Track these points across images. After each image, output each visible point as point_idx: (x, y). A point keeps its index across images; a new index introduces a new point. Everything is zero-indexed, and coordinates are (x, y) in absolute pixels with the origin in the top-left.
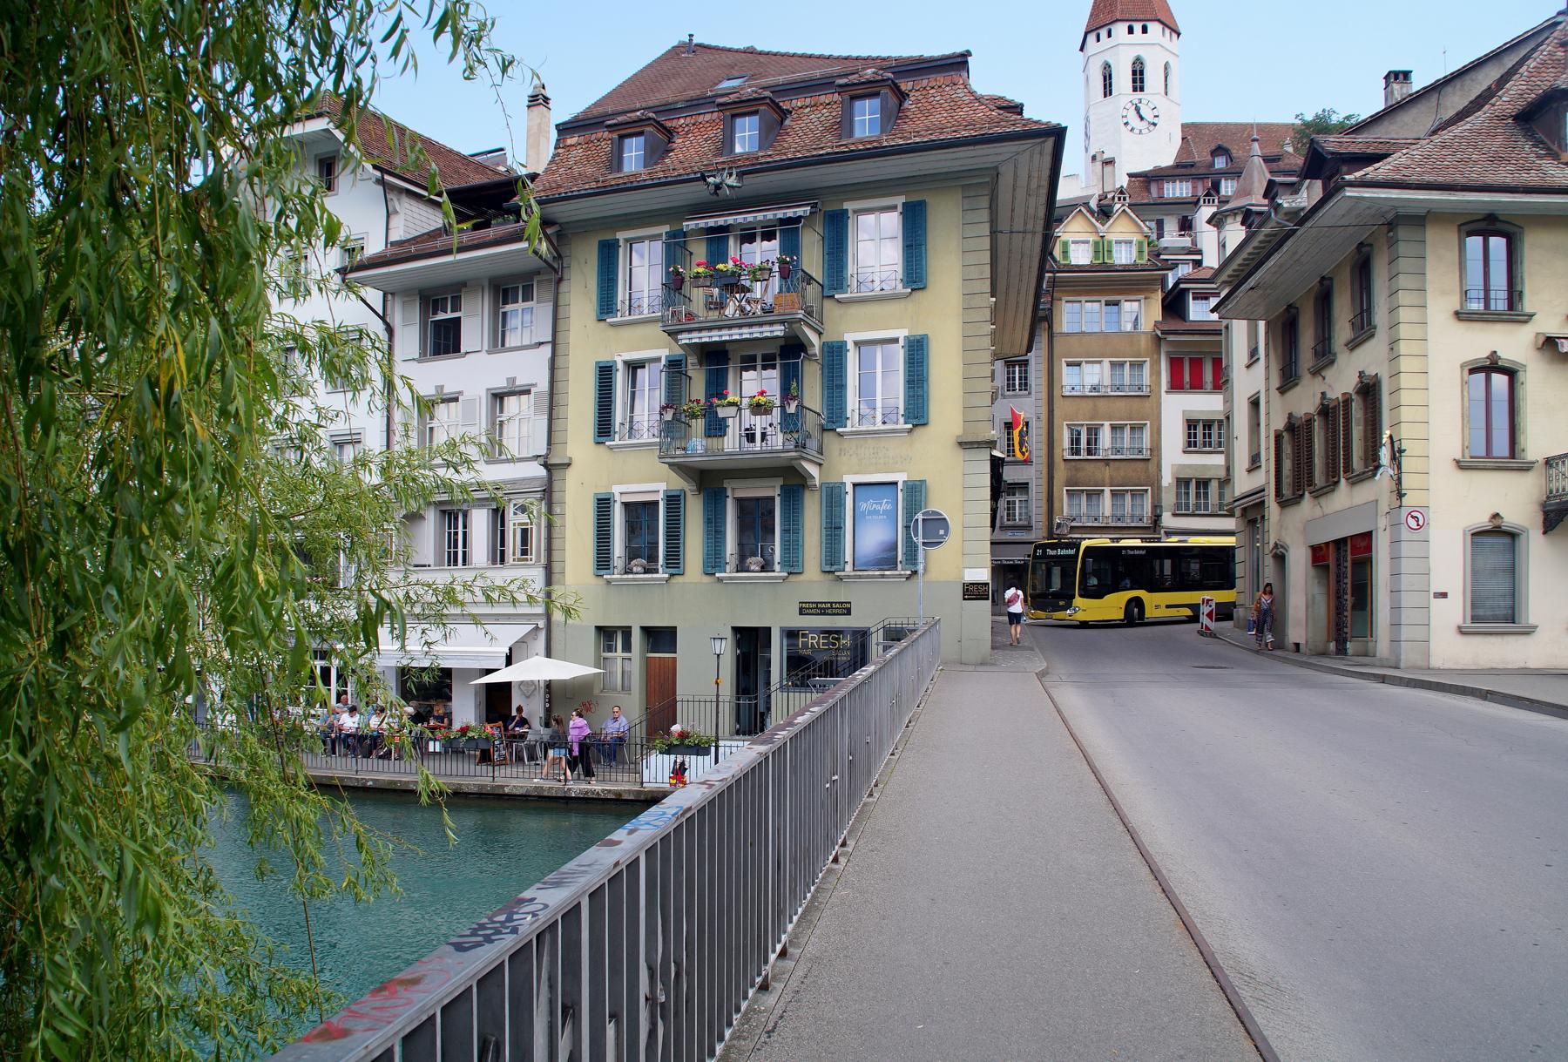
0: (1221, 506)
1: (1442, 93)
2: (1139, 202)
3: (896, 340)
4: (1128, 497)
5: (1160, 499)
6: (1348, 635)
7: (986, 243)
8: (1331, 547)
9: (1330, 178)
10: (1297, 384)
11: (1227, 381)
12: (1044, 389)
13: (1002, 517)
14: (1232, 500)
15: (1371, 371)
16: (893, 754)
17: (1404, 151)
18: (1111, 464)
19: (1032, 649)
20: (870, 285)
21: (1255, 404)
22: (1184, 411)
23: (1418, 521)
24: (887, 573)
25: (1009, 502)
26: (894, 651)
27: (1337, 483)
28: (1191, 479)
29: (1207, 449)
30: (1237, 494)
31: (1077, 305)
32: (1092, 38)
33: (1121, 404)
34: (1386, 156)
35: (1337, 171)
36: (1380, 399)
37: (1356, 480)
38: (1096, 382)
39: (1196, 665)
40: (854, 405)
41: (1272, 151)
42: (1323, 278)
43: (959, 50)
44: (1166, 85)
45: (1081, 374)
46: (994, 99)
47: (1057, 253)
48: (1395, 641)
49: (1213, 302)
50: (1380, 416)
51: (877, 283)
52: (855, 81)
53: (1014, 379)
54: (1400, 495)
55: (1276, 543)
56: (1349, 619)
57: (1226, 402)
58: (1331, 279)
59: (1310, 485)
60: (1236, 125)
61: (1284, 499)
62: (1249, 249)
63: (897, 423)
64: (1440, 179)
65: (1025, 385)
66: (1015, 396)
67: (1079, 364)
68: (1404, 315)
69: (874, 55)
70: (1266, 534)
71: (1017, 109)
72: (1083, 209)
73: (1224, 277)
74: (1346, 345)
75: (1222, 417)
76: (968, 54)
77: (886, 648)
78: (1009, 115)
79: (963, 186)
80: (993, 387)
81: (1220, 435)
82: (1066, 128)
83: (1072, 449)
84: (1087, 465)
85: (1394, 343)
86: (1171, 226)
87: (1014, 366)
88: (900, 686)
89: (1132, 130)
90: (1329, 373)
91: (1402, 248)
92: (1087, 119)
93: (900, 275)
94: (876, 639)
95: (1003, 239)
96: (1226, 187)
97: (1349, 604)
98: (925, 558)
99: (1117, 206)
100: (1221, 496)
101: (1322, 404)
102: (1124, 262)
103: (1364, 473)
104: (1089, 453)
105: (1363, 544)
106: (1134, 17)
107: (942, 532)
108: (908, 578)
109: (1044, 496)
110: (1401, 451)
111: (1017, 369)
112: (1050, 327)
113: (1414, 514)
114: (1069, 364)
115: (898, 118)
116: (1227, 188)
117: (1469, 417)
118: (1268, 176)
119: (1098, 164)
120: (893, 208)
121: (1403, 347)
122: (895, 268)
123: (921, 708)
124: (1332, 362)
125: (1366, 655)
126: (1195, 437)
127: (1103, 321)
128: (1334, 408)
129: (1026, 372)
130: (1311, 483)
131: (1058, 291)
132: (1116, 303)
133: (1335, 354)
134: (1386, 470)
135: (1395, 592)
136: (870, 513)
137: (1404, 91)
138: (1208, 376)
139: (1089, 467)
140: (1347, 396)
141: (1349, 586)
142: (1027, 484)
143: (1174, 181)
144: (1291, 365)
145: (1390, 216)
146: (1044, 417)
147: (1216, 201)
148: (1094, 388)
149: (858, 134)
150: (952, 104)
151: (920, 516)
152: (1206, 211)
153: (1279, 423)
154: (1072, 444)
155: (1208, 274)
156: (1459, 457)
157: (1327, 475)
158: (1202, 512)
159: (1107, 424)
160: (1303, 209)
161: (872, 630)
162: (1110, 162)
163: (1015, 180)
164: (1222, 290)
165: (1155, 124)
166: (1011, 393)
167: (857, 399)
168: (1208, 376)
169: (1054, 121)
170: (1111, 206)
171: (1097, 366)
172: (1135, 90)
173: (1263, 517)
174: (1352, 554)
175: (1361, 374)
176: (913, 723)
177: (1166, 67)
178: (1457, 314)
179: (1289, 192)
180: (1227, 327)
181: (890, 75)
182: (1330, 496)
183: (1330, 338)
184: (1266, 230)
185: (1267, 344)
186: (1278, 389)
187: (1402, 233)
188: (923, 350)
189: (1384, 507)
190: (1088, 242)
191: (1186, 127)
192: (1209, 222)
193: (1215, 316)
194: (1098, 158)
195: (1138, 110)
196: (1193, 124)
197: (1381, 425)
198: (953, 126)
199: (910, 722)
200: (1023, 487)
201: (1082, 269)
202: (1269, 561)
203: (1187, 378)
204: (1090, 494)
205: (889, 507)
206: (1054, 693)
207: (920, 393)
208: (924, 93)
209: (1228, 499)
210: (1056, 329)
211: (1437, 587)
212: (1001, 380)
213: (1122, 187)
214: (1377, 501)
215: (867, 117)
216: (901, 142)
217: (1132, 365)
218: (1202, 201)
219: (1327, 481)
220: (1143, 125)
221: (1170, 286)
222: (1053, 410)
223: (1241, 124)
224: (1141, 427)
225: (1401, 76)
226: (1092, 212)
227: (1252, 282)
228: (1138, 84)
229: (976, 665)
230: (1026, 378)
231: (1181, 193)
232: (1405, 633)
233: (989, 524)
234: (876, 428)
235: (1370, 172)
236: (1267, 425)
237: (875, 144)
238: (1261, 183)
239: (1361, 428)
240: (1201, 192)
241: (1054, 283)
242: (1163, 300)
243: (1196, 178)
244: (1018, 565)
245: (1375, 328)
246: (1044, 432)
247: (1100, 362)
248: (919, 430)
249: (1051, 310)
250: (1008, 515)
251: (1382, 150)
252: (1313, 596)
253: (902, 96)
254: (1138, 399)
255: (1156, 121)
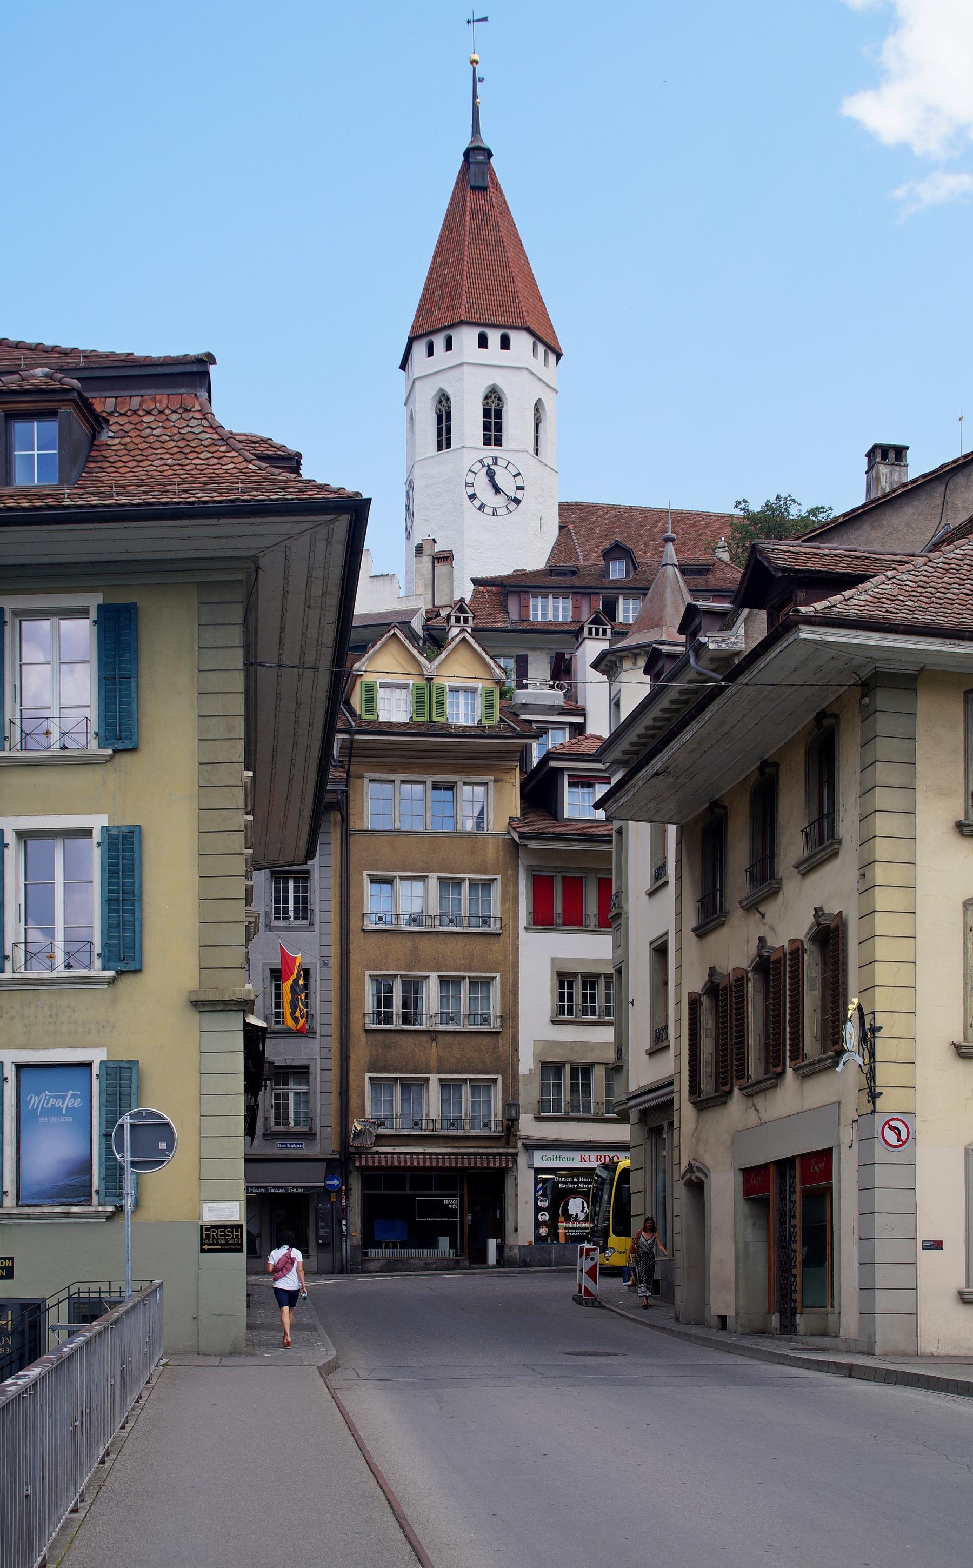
0: (609, 1106)
1: (951, 485)
2: (489, 626)
3: (87, 833)
4: (467, 1091)
5: (516, 1093)
6: (798, 1304)
7: (238, 682)
8: (772, 1172)
9: (779, 609)
10: (722, 924)
11: (618, 915)
12: (334, 918)
13: (266, 1119)
14: (624, 1097)
15: (832, 908)
16: (75, 1511)
17: (889, 574)
18: (440, 1038)
19: (314, 1328)
20: (43, 740)
21: (660, 950)
22: (553, 960)
23: (899, 1134)
24: (75, 1209)
25: (277, 1096)
26: (78, 1340)
27: (782, 1074)
28: (564, 1064)
29: (589, 1018)
30: (633, 1088)
31: (388, 787)
32: (420, 349)
33: (455, 947)
34: (863, 579)
35: (791, 597)
36: (845, 951)
37: (808, 1072)
38: (417, 909)
39: (568, 1350)
40: (17, 934)
41: (697, 556)
42: (764, 764)
43: (195, 350)
44: (537, 439)
45: (394, 897)
46: (253, 442)
47: (357, 701)
48: (867, 1313)
49: (600, 790)
50: (845, 976)
51: (55, 737)
52: (14, 387)
53: (286, 900)
54: (874, 1096)
55: (690, 1165)
56: (798, 1279)
57: (616, 947)
58: (776, 765)
59: (740, 1078)
60: (644, 511)
61: (702, 1097)
62: (655, 712)
63: (90, 967)
64: (940, 620)
65: (303, 911)
66: (288, 928)
67: (389, 881)
68: (882, 824)
69: (49, 342)
70: (676, 1151)
71: (292, 462)
72: (398, 633)
73: (616, 753)
74: (796, 867)
75: (611, 970)
76: (209, 359)
77: (71, 1333)
78: (277, 471)
79: (200, 585)
80: (248, 915)
81: (608, 997)
82: (370, 500)
83: (379, 1013)
84: (401, 1039)
85: (866, 866)
86: (539, 669)
87: (286, 881)
88: (90, 1398)
89: (481, 507)
90: (772, 909)
91: (883, 723)
92: (410, 485)
93: (94, 726)
94: (58, 1316)
95: (266, 677)
96: (626, 610)
97: (799, 1257)
98: (138, 1186)
99: (455, 631)
100: (609, 1090)
101: (760, 955)
102: (462, 721)
103: (820, 1061)
104: (406, 1021)
105: (819, 1167)
106: (488, 319)
107: (163, 1145)
108: (110, 1217)
109: (334, 1087)
110: (875, 1029)
111: (291, 885)
112: (345, 820)
113: (894, 1123)
114: (374, 880)
115: (90, 459)
116: (627, 611)
117: (3, 1467)
118: (688, 599)
119: (426, 561)
120: (81, 613)
121: (880, 874)
122: (87, 713)
123: (128, 1430)
124: (775, 892)
125: (825, 1334)
126: (570, 999)
127: (429, 815)
128: (778, 961)
129: (305, 889)
130: (742, 1072)
131: (359, 764)
132: (450, 787)
133: (780, 880)
134: (853, 1059)
135: (866, 1239)
136: (47, 1112)
137: (896, 477)
138: (591, 907)
139: (407, 1043)
140: (798, 944)
141: (798, 1230)
142: (307, 1067)
143: (545, 597)
144: (763, 860)
145: (865, 673)
146: (334, 962)
147: (609, 631)
148: (414, 920)
149: (20, 480)
150: (182, 444)
151: (126, 1120)
152: (592, 648)
153: (695, 982)
154: (379, 1006)
155: (592, 747)
156: (959, 1039)
157: (767, 1063)
158: (581, 1115)
159: (434, 976)
160: (738, 653)
161: (50, 1302)
162: (445, 558)
163: (286, 580)
164: (614, 773)
165: (517, 501)
166: (281, 923)
167: (22, 926)
168: (591, 907)
169: (351, 488)
170: (445, 630)
171: (418, 886)
172: (487, 442)
173: (671, 1124)
174: (803, 1182)
175: (818, 912)
176: (113, 1456)
177: (538, 408)
178: (959, 826)
179: (718, 625)
180: (620, 832)
181: (75, 382)
182: (770, 1094)
183: (772, 856)
184: (680, 684)
185: (679, 861)
186: (694, 930)
187: (883, 699)
188: (132, 850)
189: (849, 1113)
190: (405, 687)
191: (565, 509)
192: (595, 665)
193: (601, 814)
194: (427, 550)
195: (491, 475)
196: (576, 504)
197: (845, 990)
198: (184, 482)
199: (107, 1454)
200: (301, 1072)
201: (396, 729)
202: (680, 1190)
203: (558, 908)
204: (407, 1085)
205: (77, 1103)
206: (343, 1396)
207: (129, 920)
208: (135, 419)
209: (619, 1096)
210: (354, 824)
211: (926, 1233)
212: (263, 903)
213: (462, 600)
214: (839, 1103)
215: (36, 452)
216: (95, 501)
217: (474, 884)
218: (586, 630)
219: (767, 1071)
220: (499, 501)
221: (535, 762)
222: (348, 952)
223: (651, 511)
224: (487, 983)
225: (892, 455)
226: (412, 637)
227: (657, 764)
228: (493, 433)
229: (222, 1355)
230: (305, 900)
231: (556, 616)
232: (882, 1301)
233: (241, 1131)
234: (54, 975)
235: (837, 602)
236: (679, 985)
237: (50, 501)
238: (676, 608)
239: (817, 993)
240: (586, 616)
241: (350, 749)
242: (523, 786)
243: (580, 592)
244: (293, 1194)
245: (840, 842)
246: (334, 985)
247: (423, 879)
248: (128, 981)
249: (346, 793)
250: (277, 1115)
251: (858, 569)
252: (746, 1245)
253: (97, 422)
254: (482, 939)
255: (519, 495)
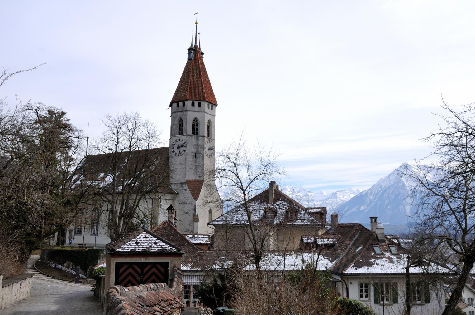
123: (19, 292)
228: (195, 131)
